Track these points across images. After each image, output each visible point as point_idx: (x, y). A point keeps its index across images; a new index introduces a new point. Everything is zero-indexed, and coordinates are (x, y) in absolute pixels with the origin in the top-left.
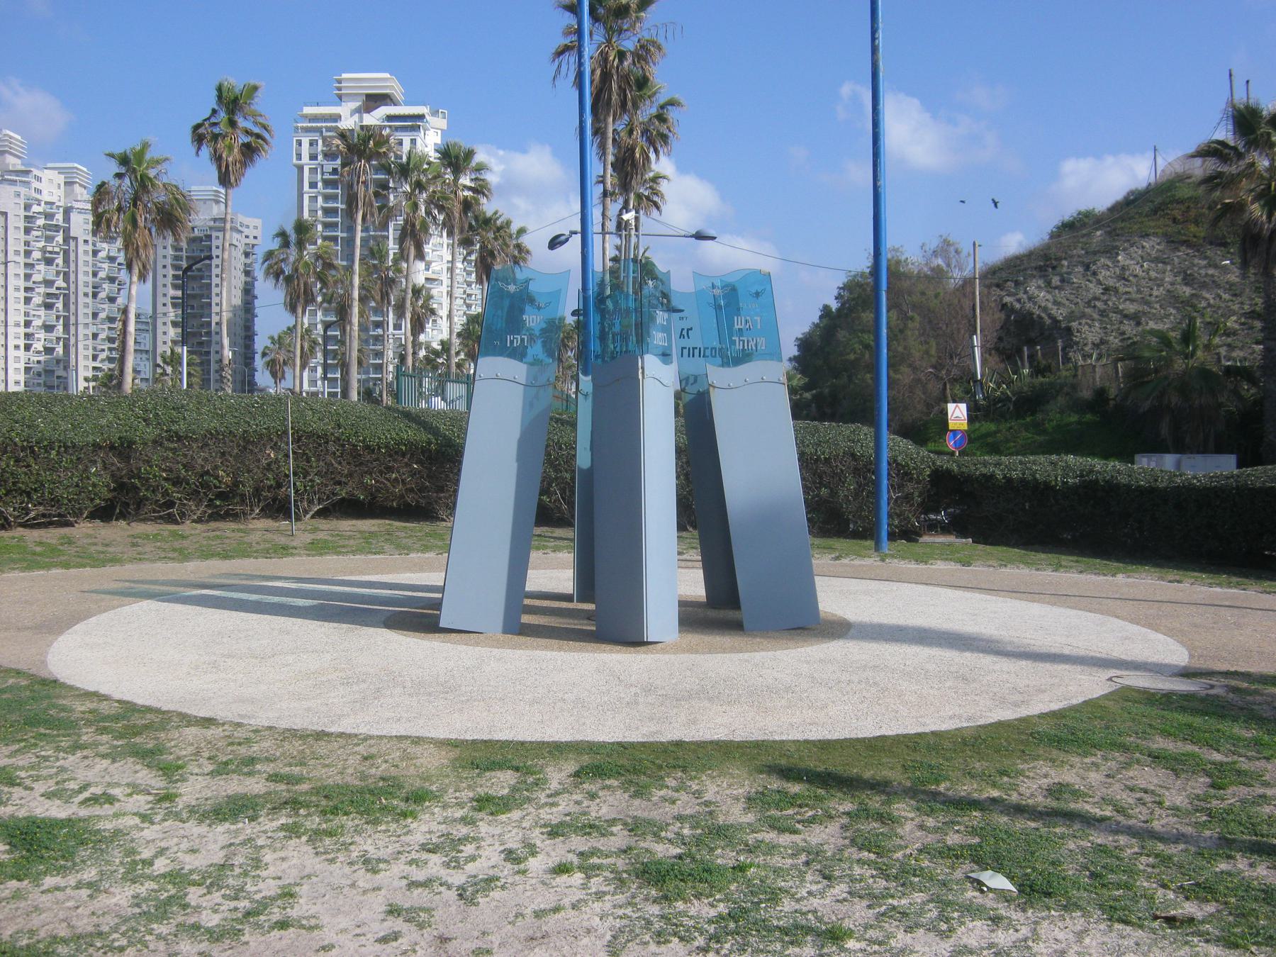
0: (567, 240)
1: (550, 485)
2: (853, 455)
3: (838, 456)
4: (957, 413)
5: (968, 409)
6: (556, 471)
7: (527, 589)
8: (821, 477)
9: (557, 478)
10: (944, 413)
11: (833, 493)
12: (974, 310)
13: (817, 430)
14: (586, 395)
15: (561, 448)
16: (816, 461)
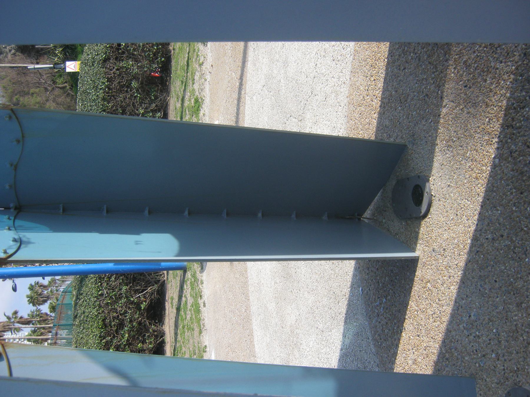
0: (15, 285)
1: (132, 303)
2: (105, 60)
3: (105, 73)
4: (72, 67)
5: (69, 61)
6: (120, 298)
7: (398, 369)
8: (123, 86)
9: (127, 297)
10: (69, 73)
11: (135, 78)
12: (13, 67)
13: (85, 92)
14: (20, 243)
15: (102, 295)
16: (109, 89)
